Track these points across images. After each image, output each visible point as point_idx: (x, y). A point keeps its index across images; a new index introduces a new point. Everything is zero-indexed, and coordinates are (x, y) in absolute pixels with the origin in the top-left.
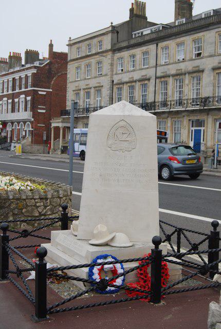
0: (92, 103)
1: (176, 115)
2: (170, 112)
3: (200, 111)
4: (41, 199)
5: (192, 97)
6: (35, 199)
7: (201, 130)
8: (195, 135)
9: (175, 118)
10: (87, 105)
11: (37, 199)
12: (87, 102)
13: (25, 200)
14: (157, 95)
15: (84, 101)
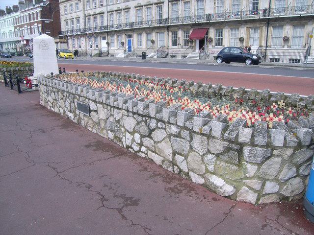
0: (69, 27)
5: (184, 16)
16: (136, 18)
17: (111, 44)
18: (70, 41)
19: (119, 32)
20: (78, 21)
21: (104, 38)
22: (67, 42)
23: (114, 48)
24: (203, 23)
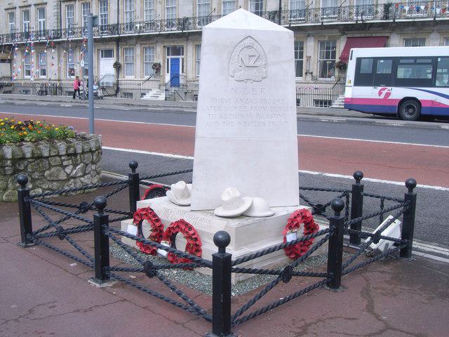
0: (18, 26)
1: (146, 40)
2: (139, 37)
3: (110, 40)
4: (68, 155)
5: (321, 6)
6: (60, 156)
7: (179, 59)
8: (171, 66)
9: (146, 44)
10: (26, 28)
11: (63, 156)
12: (25, 24)
13: (47, 158)
14: (120, 16)
15: (21, 23)
16: (194, 9)
17: (124, 67)
18: (18, 58)
19: (146, 40)
20: (42, 12)
21: (108, 54)
22: (10, 61)
23: (132, 77)
24: (372, 25)
